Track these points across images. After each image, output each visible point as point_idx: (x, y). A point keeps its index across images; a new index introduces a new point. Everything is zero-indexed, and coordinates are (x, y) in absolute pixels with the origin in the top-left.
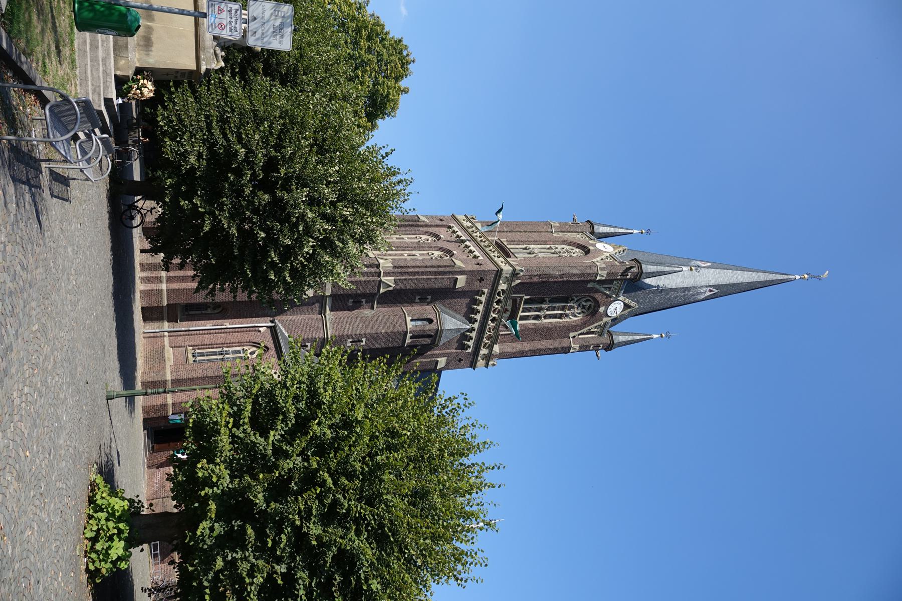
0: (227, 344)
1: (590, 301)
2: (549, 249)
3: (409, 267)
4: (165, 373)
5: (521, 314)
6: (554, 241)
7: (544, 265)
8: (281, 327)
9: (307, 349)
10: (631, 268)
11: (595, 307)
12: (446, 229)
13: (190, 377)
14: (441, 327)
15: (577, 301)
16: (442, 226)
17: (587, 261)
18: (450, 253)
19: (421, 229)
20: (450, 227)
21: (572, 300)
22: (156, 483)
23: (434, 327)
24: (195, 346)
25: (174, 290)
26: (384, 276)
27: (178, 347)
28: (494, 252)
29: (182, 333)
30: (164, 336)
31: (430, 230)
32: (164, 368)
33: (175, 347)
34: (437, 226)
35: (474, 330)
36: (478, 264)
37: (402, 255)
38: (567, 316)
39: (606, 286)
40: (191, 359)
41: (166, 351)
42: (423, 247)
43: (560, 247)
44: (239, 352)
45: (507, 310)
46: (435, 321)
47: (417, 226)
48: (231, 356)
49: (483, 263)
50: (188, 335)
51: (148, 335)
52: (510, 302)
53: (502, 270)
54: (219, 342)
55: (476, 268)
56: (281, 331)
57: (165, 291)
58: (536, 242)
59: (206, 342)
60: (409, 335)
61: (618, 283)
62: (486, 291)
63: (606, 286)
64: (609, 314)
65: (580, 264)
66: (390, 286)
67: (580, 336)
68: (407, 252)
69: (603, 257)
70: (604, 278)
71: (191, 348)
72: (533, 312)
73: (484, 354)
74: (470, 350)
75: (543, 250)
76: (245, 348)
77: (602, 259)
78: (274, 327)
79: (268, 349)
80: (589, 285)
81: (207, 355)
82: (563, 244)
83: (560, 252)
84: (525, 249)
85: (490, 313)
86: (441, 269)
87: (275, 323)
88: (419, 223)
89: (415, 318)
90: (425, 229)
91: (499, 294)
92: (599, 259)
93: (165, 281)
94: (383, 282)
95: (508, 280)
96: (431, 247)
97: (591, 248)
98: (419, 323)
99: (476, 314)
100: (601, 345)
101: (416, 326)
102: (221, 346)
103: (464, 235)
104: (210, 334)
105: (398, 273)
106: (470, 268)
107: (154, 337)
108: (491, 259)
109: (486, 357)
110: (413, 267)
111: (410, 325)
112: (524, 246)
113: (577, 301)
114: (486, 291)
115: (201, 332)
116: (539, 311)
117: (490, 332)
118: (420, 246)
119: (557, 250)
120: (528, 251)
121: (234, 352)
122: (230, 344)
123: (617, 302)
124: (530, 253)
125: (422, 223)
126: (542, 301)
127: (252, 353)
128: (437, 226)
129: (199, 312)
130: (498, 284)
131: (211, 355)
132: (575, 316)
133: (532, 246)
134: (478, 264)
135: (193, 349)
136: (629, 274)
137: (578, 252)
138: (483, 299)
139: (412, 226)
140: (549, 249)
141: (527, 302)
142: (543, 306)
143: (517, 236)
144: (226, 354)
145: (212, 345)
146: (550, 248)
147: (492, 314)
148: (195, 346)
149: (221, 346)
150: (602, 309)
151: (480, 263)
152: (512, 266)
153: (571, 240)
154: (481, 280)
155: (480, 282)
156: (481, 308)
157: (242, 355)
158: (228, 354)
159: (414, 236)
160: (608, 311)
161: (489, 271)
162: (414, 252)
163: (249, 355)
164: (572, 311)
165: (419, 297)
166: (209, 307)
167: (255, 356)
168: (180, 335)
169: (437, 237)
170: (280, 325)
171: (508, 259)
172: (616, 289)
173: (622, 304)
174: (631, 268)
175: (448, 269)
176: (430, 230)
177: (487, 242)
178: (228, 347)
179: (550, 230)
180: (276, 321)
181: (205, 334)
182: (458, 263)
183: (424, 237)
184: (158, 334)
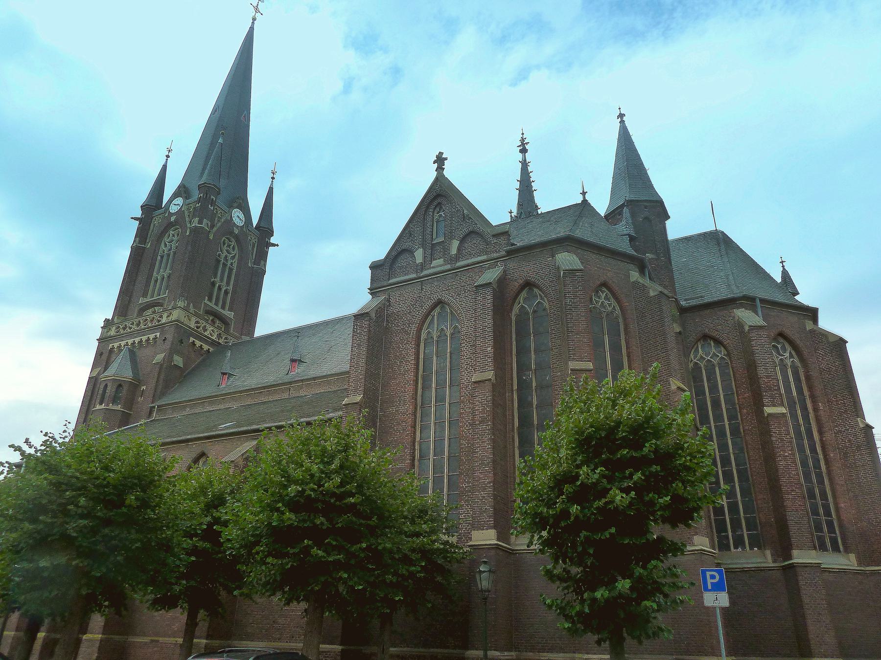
21: (219, 255)
38: (232, 264)
75: (163, 265)
126: (213, 284)
173: (236, 210)
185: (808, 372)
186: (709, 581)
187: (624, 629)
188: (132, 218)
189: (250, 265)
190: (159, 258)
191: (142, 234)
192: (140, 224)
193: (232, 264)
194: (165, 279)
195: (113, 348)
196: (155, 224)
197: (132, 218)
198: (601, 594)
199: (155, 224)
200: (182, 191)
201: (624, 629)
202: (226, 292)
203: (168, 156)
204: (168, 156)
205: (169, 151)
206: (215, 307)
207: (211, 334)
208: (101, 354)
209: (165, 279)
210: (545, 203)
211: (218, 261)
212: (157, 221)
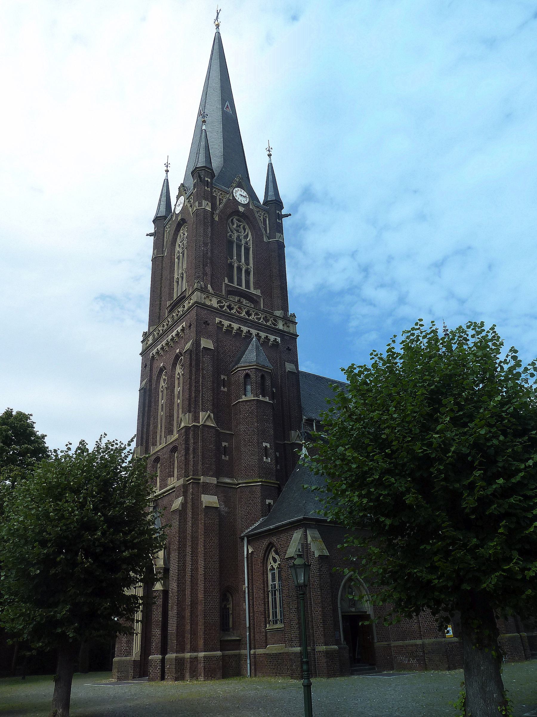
0: (264, 587)
1: (232, 220)
2: (179, 259)
3: (190, 396)
4: (293, 653)
5: (243, 287)
6: (171, 255)
7: (194, 261)
8: (249, 530)
9: (272, 504)
10: (200, 177)
11: (238, 215)
12: (155, 361)
13: (297, 626)
14: (254, 365)
15: (232, 232)
16: (151, 365)
17: (191, 219)
18: (177, 357)
19: (154, 386)
20: (153, 357)
21: (230, 236)
22: (409, 660)
23: (253, 372)
24: (265, 621)
25: (205, 644)
26: (199, 422)
27: (266, 639)
28: (179, 312)
29: (252, 635)
30: (255, 654)
31: (155, 377)
32: (287, 654)
33: (266, 643)
34: (151, 370)
35: (258, 333)
36: (190, 326)
37: (178, 405)
38: (247, 243)
39: (218, 203)
40: (279, 626)
41: (270, 652)
42: (171, 384)
43: (177, 249)
44: (273, 575)
45: (239, 301)
46: (247, 371)
47: (150, 390)
48: (276, 583)
49: (189, 322)
50: (254, 628)
51: (253, 671)
52: (231, 298)
53: (196, 302)
54: (262, 595)
55: (193, 328)
56: (253, 530)
57: (206, 653)
58: (172, 272)
59: (261, 609)
60: (261, 398)
61: (215, 191)
62: (218, 320)
63: (218, 203)
64: (246, 202)
65: (195, 226)
66: (209, 416)
67: (268, 232)
68: (176, 399)
69: (189, 205)
70: (210, 204)
71: (268, 625)
72: (241, 276)
73: (283, 325)
74: (279, 339)
75: (180, 265)
76: (269, 567)
77: (191, 206)
78: (248, 537)
79: (270, 543)
80: (217, 219)
81: (276, 608)
82: (175, 246)
83: (183, 248)
84: (178, 282)
85: (241, 317)
86: (194, 363)
87: (244, 536)
88: (148, 388)
89: (243, 392)
90: (154, 382)
91: (222, 307)
92: (190, 210)
93: (196, 654)
94: (205, 422)
95: (208, 297)
96: (172, 376)
97: (179, 218)
98: (249, 387)
99: (223, 325)
100: (277, 212)
101: (252, 390)
102: (266, 593)
103: (161, 342)
104: (253, 605)
105: (195, 408)
106: (193, 335)
107: (255, 665)
108: (185, 314)
109: (286, 323)
110: (190, 392)
111: (250, 397)
112: (175, 284)
113: (232, 232)
114: (218, 320)
115: (251, 615)
116: (241, 270)
117: (260, 318)
118: (171, 388)
119: (181, 251)
120: (180, 279)
121: (273, 580)
122: (265, 582)
123: (234, 193)
124: (182, 278)
125: (148, 385)
126: (231, 266)
127: (275, 560)
128: (151, 370)
129: (231, 617)
130: (211, 307)
131: (276, 604)
132: (247, 235)
133: (176, 276)
134: (190, 326)
135: (269, 624)
136: (206, 179)
137: (184, 233)
138: (226, 323)
139: (150, 396)
140: (179, 259)
141: (231, 280)
142: (236, 265)
143: (165, 290)
144: (275, 587)
145: (266, 603)
146: (178, 258)
147: (242, 315)
148: (265, 621)
149: (266, 593)
150: (241, 209)
151: (188, 324)
152: (193, 293)
153: (171, 238)
154: (206, 323)
155: (208, 324)
156: (235, 326)
157: (276, 572)
158: (275, 585)
159: (160, 394)
160: (243, 202)
161: (197, 315)
162: (176, 393)
163: (277, 564)
164: (242, 237)
165: (222, 387)
166: (225, 605)
167: (277, 557)
168: (254, 637)
169: (161, 370)
170: (246, 531)
171: (187, 296)
172: (221, 194)
173: (236, 189)
174: (200, 177)
175: (194, 357)
176: (155, 377)
177: (169, 319)
178: (268, 586)
179: (160, 259)
180: (242, 535)
181: (253, 611)
182: (188, 346)
183: (162, 383)
184: (253, 660)
185: (266, 639)
187: (432, 585)
188: (147, 235)
190: (176, 260)
192: (155, 237)
193: (247, 243)
197: (147, 235)
200: (183, 189)
201: (432, 585)
202: (248, 273)
203: (167, 171)
204: (167, 171)
205: (167, 166)
207: (238, 312)
208: (145, 367)
211: (231, 243)
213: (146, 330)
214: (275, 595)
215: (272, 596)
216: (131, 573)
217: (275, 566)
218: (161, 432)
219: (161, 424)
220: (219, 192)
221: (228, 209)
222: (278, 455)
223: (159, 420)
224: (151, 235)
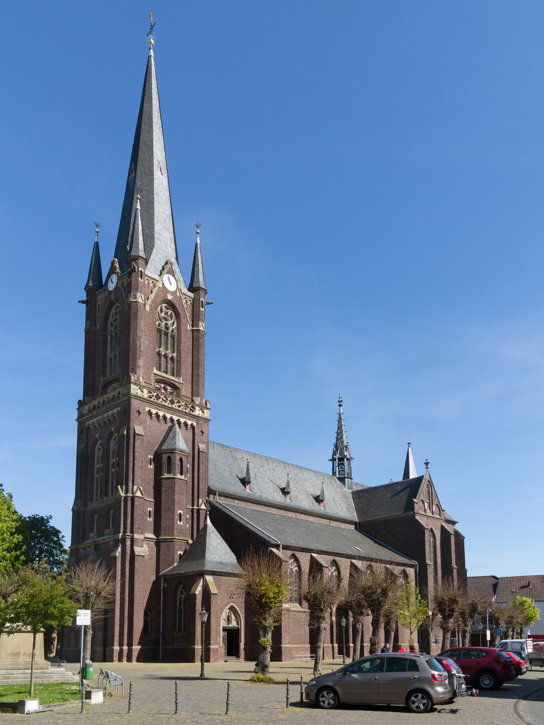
21: (159, 325)
44: (180, 602)
48: (182, 607)
76: (178, 597)
81: (181, 622)
114: (147, 409)
127: (182, 593)
144: (181, 610)
158: (181, 608)
162: (111, 463)
163: (183, 596)
170: (163, 572)
186: (498, 632)
188: (79, 302)
189: (189, 328)
190: (109, 337)
191: (90, 316)
192: (87, 307)
194: (118, 356)
195: (89, 425)
196: (99, 305)
197: (79, 302)
198: (55, 546)
199: (99, 305)
206: (164, 375)
209: (118, 356)
210: (85, 299)
212: (101, 299)
213: (81, 398)
214: (181, 614)
215: (179, 614)
216: (51, 558)
217: (183, 597)
218: (97, 491)
219: (97, 484)
220: (150, 280)
221: (158, 298)
222: (188, 517)
223: (95, 481)
224: (82, 302)
